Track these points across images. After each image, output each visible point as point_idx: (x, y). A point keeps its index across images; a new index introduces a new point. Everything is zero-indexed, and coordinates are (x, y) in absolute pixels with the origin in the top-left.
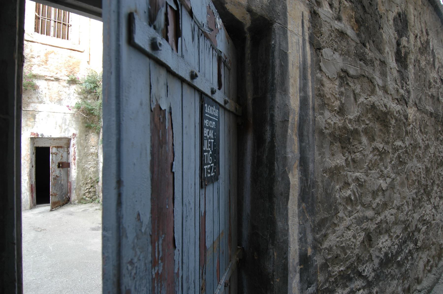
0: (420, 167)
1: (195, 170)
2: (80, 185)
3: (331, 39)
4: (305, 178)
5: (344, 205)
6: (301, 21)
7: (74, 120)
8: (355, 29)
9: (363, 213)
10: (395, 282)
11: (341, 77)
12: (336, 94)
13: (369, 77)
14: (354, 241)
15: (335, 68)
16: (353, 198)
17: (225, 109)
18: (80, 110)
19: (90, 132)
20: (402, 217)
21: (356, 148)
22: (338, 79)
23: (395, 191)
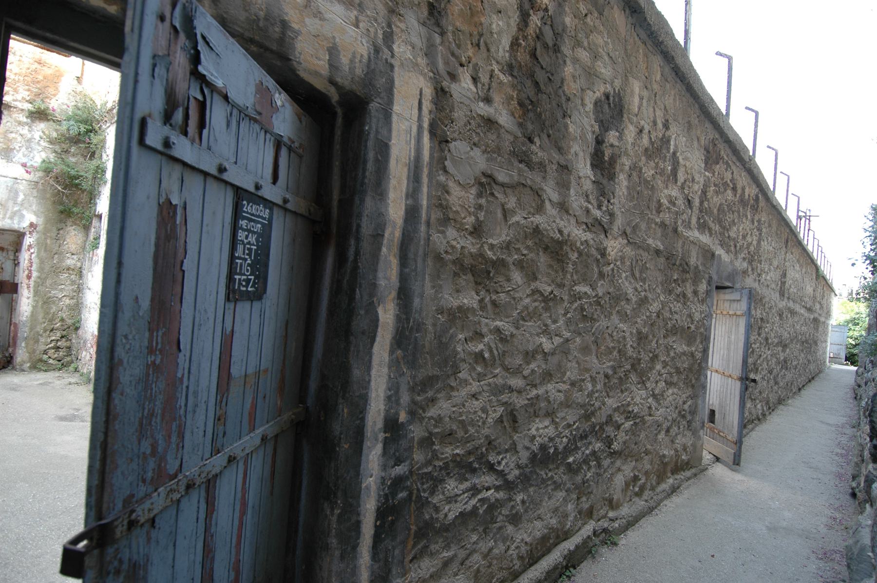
0: (625, 329)
1: (219, 277)
2: (38, 332)
3: (468, 128)
4: (405, 317)
5: (470, 364)
6: (417, 101)
7: (35, 194)
8: (517, 116)
9: (504, 379)
10: (561, 494)
11: (481, 184)
12: (470, 207)
13: (533, 187)
14: (484, 416)
15: (472, 170)
16: (486, 355)
17: (286, 210)
18: (50, 176)
19: (69, 223)
20: (579, 397)
21: (501, 286)
22: (477, 186)
23: (570, 358)
